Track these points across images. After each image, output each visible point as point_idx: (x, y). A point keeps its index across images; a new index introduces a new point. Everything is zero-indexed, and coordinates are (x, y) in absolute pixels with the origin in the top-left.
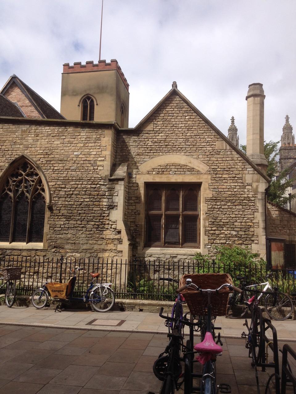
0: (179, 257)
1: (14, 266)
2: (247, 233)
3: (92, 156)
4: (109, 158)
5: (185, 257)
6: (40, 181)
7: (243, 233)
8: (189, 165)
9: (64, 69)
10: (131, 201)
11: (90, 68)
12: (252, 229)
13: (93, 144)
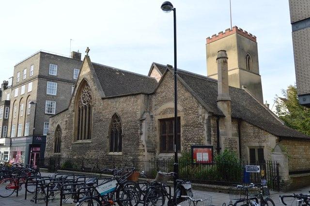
1: (209, 140)
12: (202, 141)
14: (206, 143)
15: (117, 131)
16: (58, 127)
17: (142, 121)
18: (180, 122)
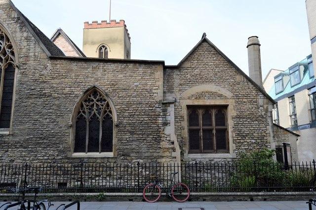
0: (216, 160)
2: (262, 140)
3: (148, 86)
4: (161, 87)
5: (220, 160)
6: (108, 105)
7: (260, 141)
8: (219, 92)
9: (85, 26)
10: (177, 120)
11: (95, 25)
12: (266, 138)
13: (149, 77)
15: (94, 118)
17: (166, 104)
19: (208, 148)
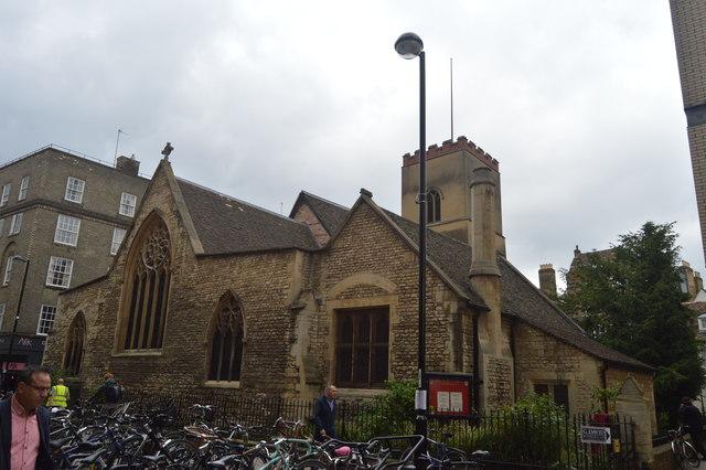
1: (458, 363)
14: (450, 367)
16: (80, 316)
18: (388, 318)
19: (360, 382)
